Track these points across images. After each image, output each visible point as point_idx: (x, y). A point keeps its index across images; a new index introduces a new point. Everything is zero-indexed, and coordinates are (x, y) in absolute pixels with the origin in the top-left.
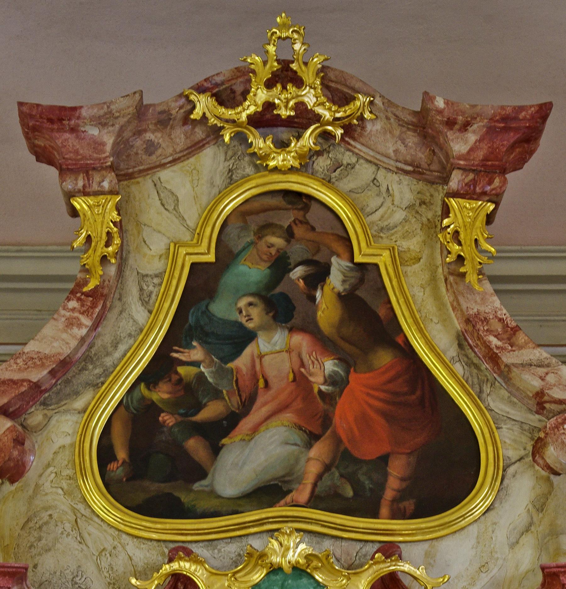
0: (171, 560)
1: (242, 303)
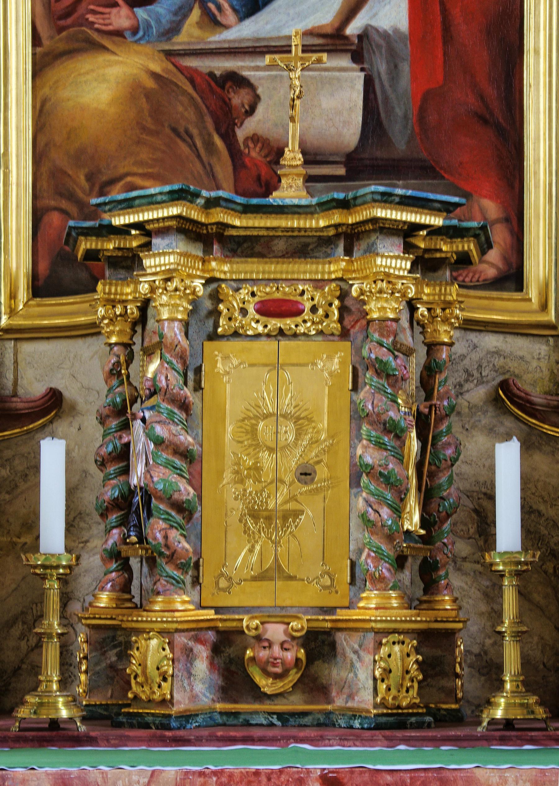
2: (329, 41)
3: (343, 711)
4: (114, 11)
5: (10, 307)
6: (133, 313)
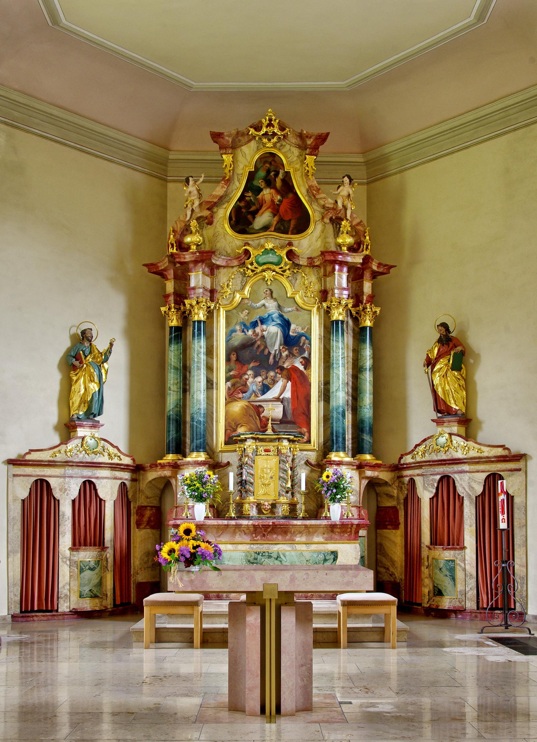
0: (244, 246)
1: (260, 182)
3: (277, 516)
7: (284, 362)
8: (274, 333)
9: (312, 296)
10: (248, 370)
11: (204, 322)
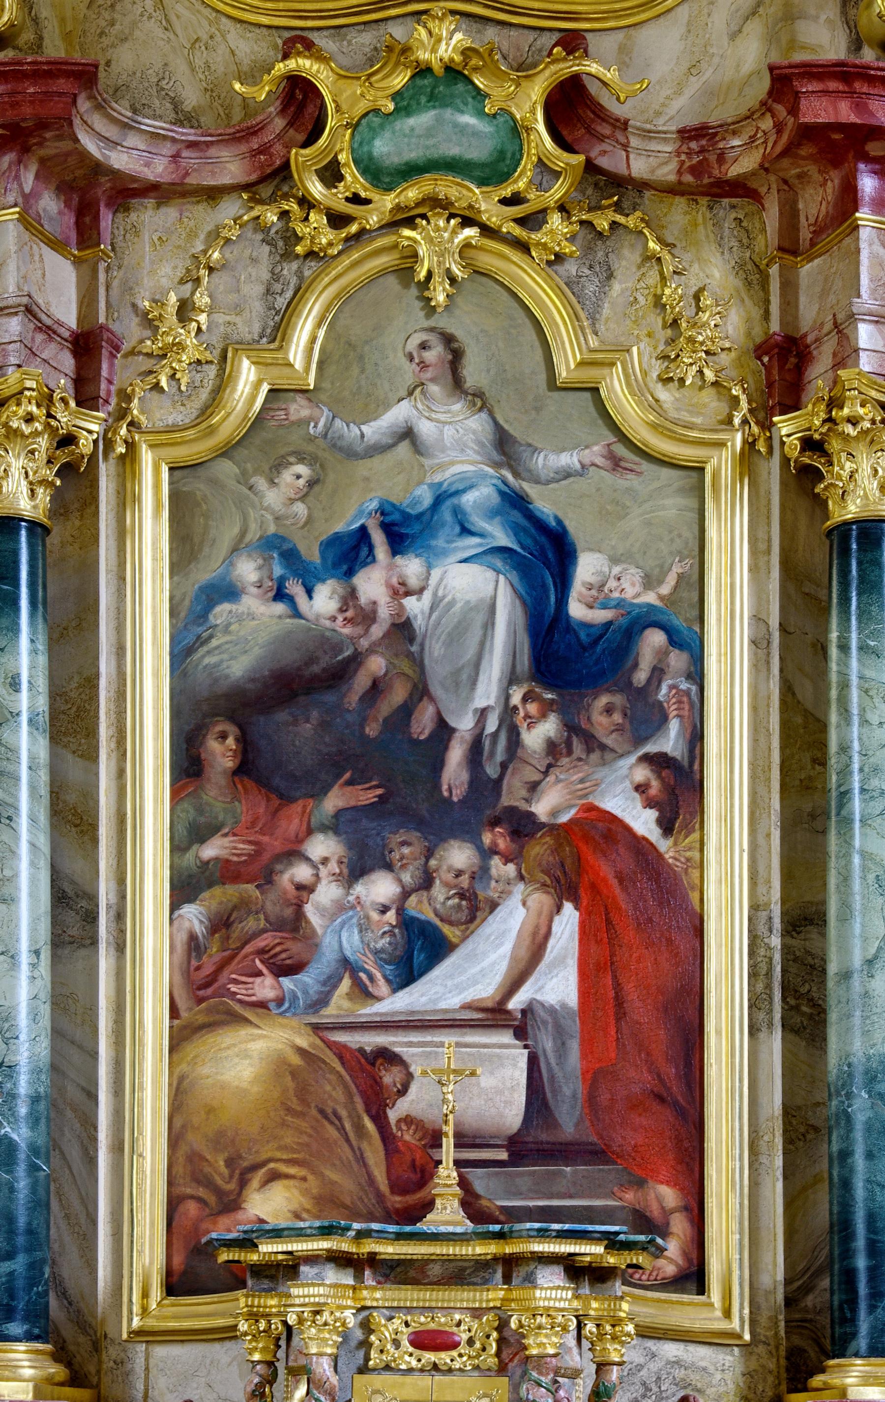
0: (286, 57)
2: (490, 1016)
4: (258, 980)
5: (143, 1305)
6: (277, 1328)
7: (534, 787)
8: (470, 608)
9: (709, 375)
10: (310, 832)
11: (34, 526)
